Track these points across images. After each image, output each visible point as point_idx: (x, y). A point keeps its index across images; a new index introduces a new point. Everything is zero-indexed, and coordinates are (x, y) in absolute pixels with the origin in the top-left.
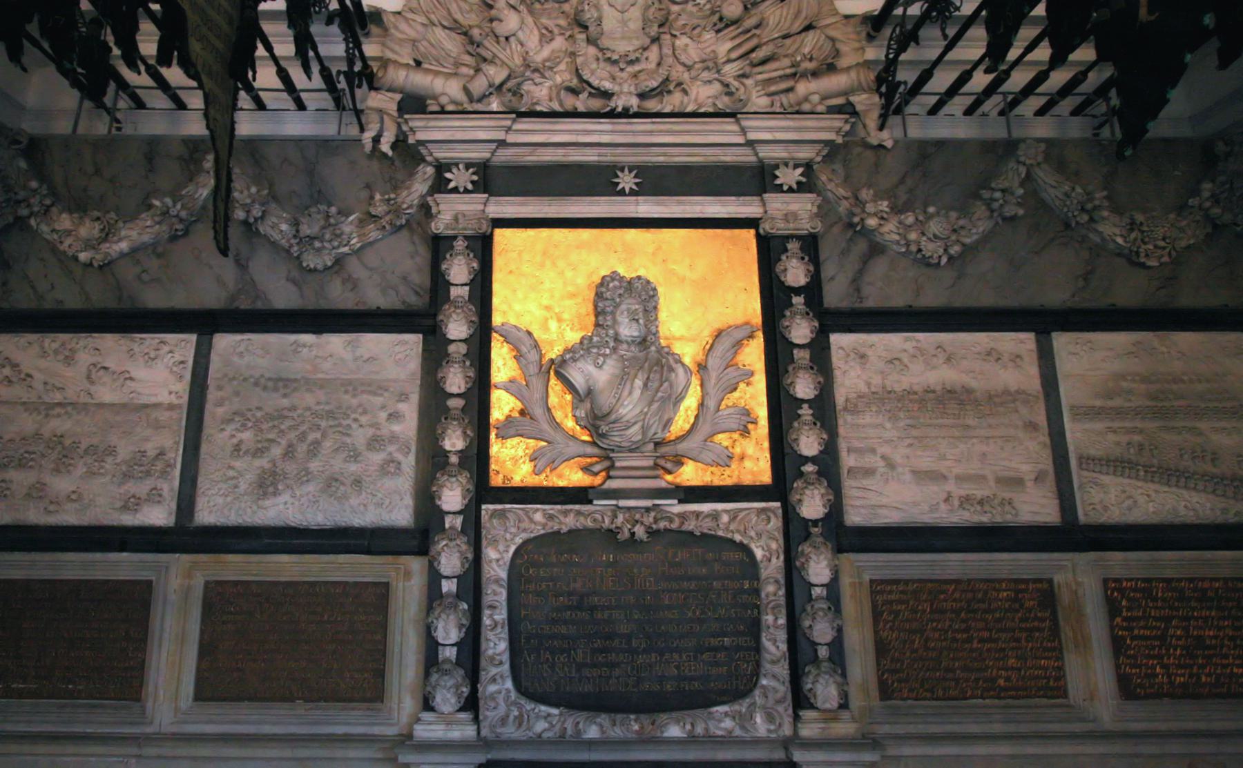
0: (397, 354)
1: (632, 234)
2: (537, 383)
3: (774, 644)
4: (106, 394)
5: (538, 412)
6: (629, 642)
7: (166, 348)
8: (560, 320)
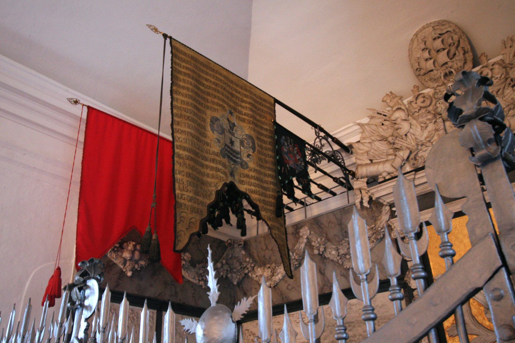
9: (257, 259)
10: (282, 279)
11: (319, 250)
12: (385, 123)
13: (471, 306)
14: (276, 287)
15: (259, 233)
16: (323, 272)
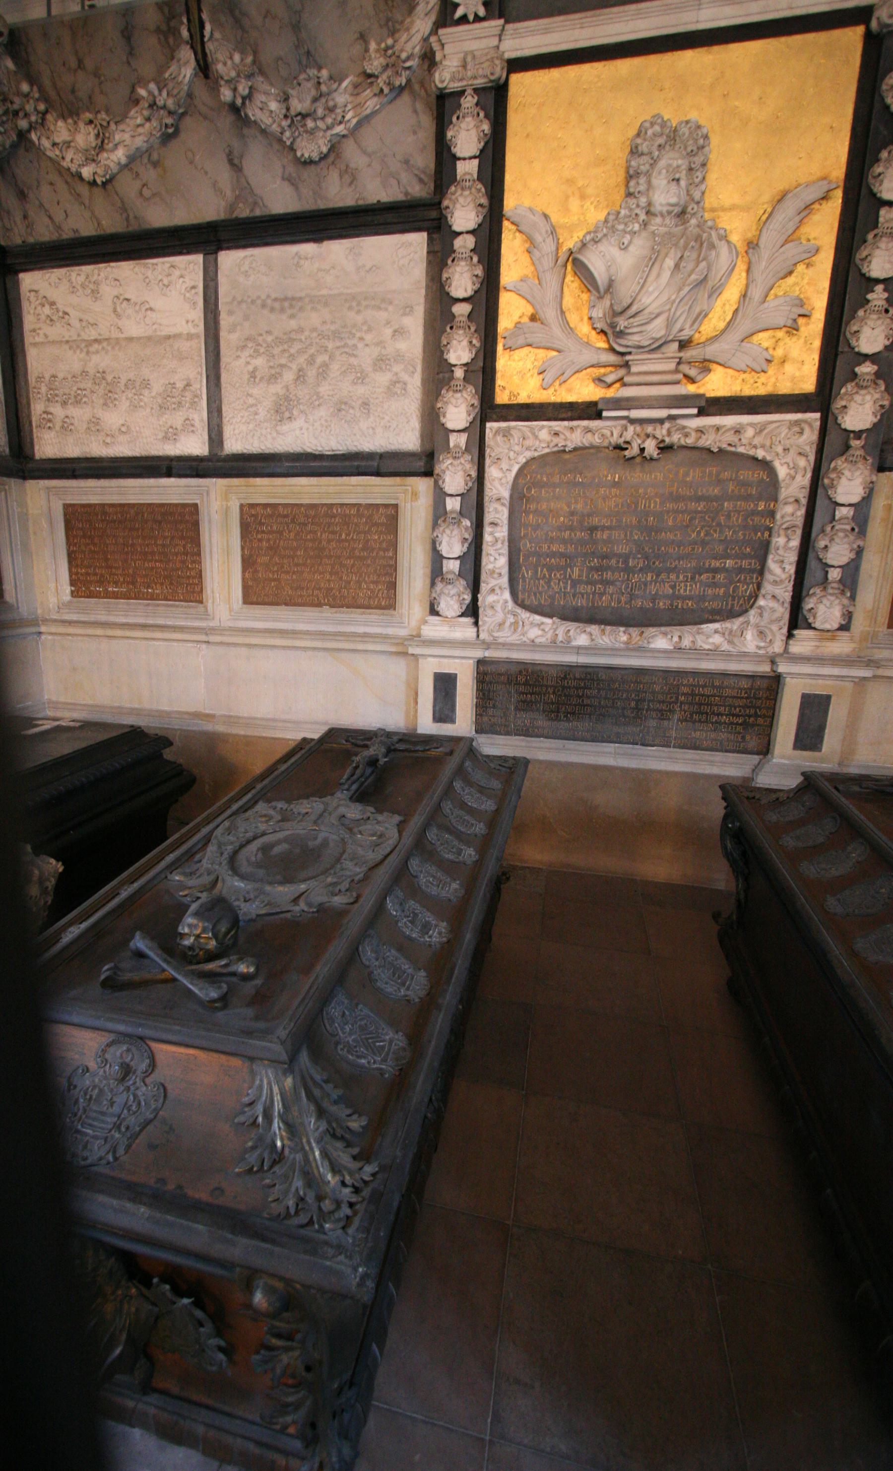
0: (401, 255)
1: (687, 58)
2: (551, 281)
4: (133, 328)
5: (550, 314)
7: (177, 273)
8: (583, 197)
9: (52, 94)
10: (126, 166)
11: (235, 90)
13: (565, 289)
14: (109, 187)
15: (54, 12)
16: (236, 161)
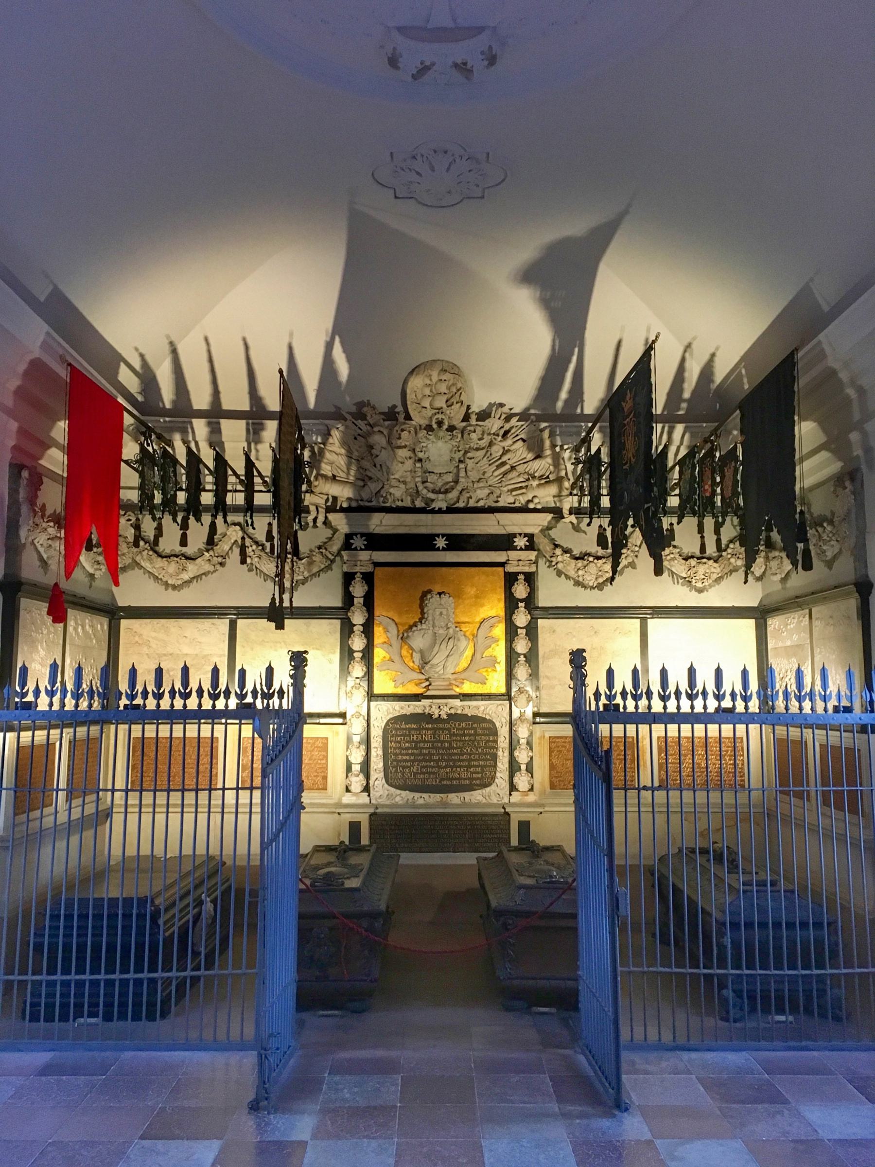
3: (503, 764)
6: (437, 763)
12: (358, 437)
